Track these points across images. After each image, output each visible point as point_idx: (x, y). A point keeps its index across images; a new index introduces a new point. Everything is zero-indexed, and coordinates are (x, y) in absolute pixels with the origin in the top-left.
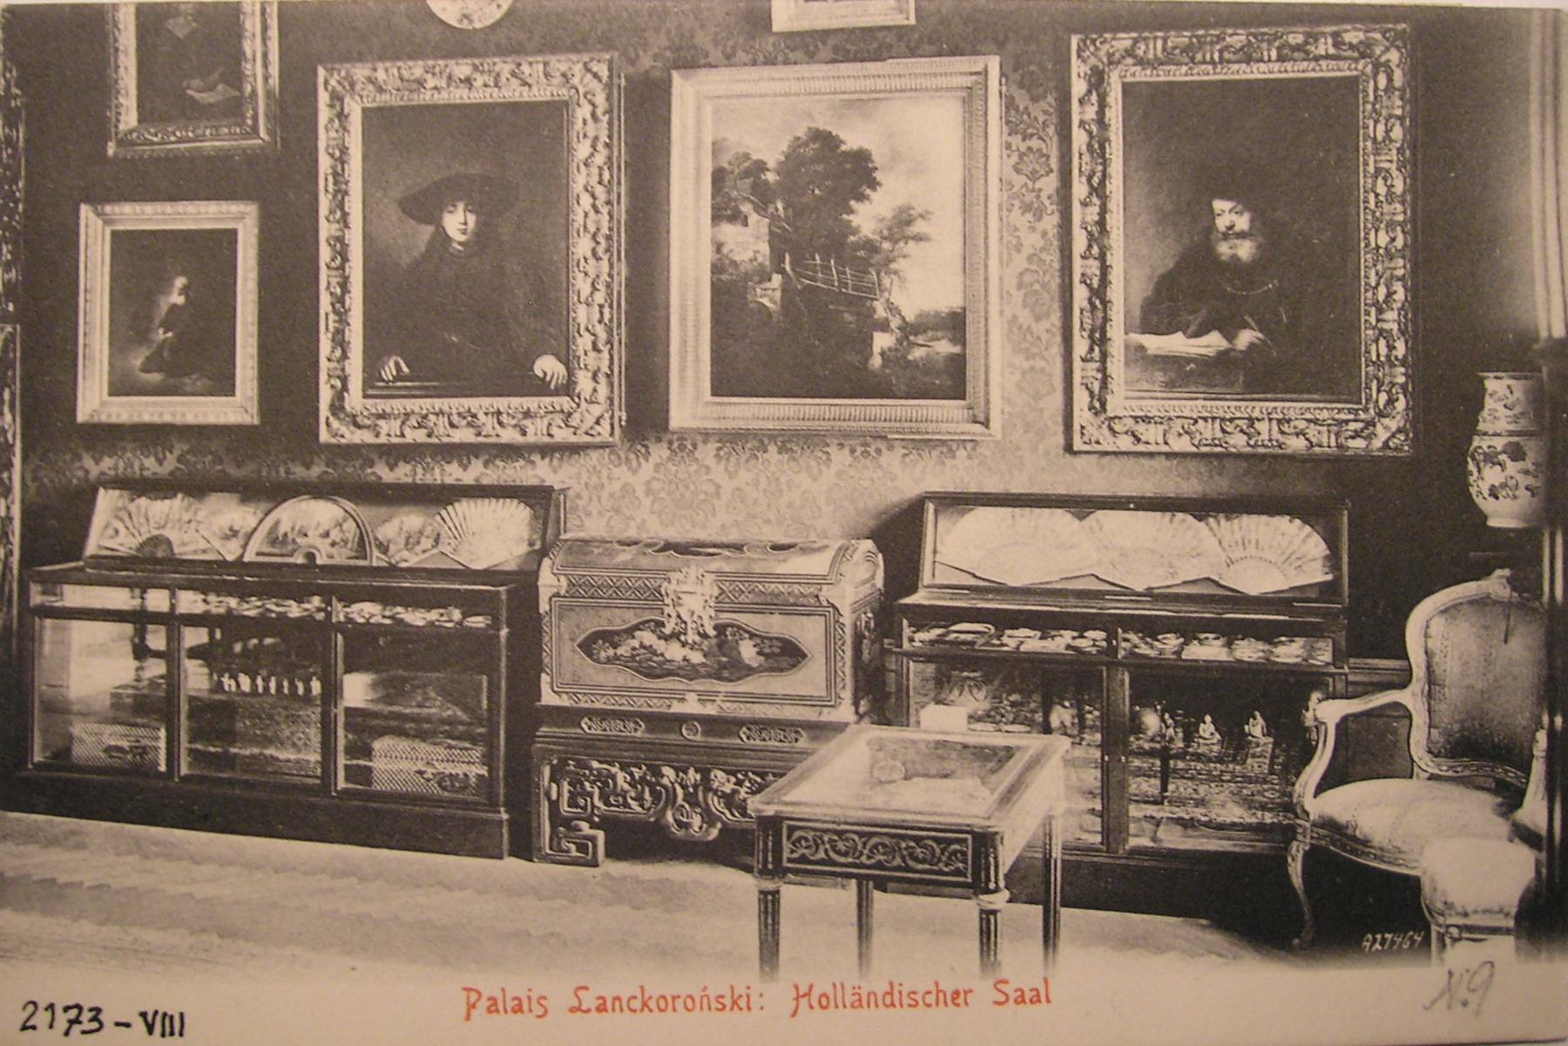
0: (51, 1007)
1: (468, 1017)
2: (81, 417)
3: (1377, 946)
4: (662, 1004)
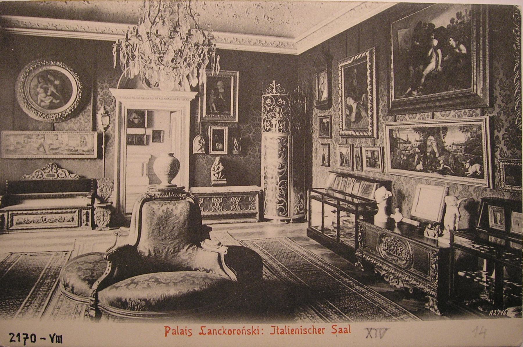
0: (19, 335)
1: (166, 335)
3: (495, 314)
4: (230, 332)
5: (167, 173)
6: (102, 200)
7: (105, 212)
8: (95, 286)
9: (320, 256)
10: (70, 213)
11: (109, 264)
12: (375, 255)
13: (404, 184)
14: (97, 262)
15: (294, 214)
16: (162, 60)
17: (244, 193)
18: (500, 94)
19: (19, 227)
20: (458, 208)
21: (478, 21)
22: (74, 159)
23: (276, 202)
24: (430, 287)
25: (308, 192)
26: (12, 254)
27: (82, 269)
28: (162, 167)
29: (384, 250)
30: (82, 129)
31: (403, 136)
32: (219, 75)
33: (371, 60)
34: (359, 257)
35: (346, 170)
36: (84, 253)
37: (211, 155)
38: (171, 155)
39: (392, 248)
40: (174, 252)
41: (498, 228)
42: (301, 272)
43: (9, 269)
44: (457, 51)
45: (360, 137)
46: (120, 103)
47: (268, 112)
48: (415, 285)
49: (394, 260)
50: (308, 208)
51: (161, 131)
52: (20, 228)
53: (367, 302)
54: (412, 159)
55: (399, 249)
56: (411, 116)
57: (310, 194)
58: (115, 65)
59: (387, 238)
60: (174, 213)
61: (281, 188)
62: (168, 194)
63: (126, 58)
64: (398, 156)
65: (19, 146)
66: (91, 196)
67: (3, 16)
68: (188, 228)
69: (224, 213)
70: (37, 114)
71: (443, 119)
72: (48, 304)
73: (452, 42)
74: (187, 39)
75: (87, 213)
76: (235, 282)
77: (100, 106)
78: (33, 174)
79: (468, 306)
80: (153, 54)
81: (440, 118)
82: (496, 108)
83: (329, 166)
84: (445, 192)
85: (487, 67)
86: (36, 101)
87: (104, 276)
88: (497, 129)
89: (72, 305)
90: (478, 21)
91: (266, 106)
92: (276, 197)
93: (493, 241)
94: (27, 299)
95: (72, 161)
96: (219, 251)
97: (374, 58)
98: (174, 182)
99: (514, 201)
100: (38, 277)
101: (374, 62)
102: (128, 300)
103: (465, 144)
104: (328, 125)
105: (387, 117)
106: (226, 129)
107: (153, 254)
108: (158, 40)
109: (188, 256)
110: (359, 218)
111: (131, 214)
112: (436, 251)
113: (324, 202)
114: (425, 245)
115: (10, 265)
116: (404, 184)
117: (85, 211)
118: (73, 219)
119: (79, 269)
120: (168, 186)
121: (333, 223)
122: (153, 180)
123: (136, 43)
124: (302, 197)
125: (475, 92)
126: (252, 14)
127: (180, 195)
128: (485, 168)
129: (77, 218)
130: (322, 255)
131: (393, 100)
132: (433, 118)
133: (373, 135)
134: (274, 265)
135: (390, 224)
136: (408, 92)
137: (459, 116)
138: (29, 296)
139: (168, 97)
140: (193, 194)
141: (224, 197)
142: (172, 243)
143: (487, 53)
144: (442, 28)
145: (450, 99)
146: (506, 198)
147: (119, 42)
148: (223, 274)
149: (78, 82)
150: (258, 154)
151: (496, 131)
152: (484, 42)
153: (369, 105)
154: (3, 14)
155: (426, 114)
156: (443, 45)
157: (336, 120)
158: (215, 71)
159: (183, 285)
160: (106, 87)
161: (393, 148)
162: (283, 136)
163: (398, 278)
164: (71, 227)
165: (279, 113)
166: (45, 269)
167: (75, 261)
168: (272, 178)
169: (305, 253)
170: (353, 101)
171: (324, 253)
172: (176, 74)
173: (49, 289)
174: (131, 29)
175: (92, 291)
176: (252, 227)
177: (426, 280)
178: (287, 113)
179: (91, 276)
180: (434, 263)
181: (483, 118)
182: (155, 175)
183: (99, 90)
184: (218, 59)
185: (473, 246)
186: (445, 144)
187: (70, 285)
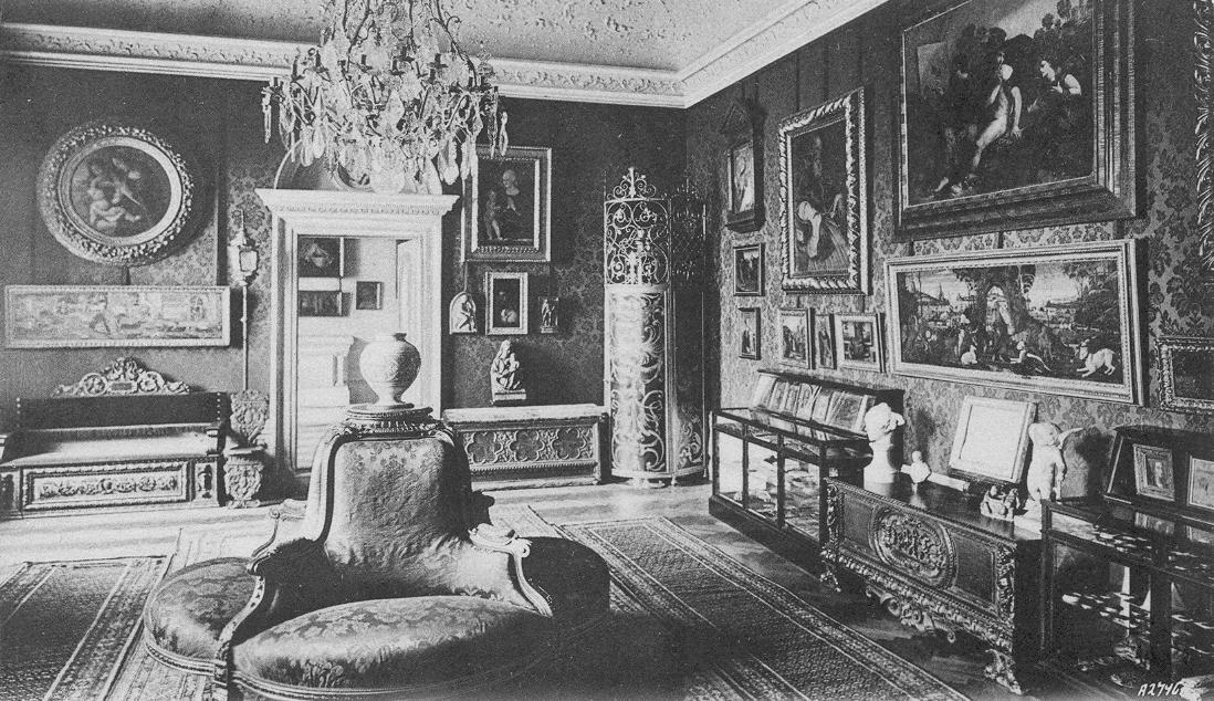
5: (392, 378)
6: (242, 440)
7: (249, 468)
8: (227, 633)
9: (741, 560)
10: (168, 469)
11: (259, 582)
12: (866, 558)
13: (932, 398)
14: (231, 579)
15: (679, 467)
16: (376, 124)
17: (565, 421)
18: (1162, 186)
19: (48, 503)
20: (1062, 451)
21: (1109, 19)
22: (175, 348)
23: (639, 441)
24: (996, 629)
25: (710, 417)
26: (30, 564)
27: (197, 596)
28: (378, 366)
29: (887, 545)
30: (195, 282)
31: (929, 288)
32: (506, 156)
33: (855, 119)
34: (829, 560)
35: (798, 366)
36: (200, 560)
37: (490, 336)
38: (400, 337)
39: (906, 540)
40: (408, 553)
41: (1156, 496)
42: (695, 594)
43: (25, 600)
44: (1060, 89)
45: (830, 292)
46: (282, 222)
47: (619, 238)
48: (960, 624)
49: (911, 568)
50: (710, 453)
51: (376, 283)
52: (50, 506)
53: (849, 662)
54: (953, 340)
55: (923, 542)
56: (947, 242)
57: (714, 420)
58: (268, 137)
59: (893, 518)
60: (408, 467)
61: (650, 407)
62: (393, 426)
63: (294, 119)
64: (917, 334)
65: (46, 321)
66: (216, 433)
67: (6, 25)
68: (441, 499)
69: (521, 464)
70: (90, 246)
71: (1024, 247)
72: (116, 677)
73: (1047, 70)
74: (433, 77)
75: (208, 470)
76: (549, 619)
77: (235, 228)
78: (81, 384)
79: (1087, 672)
80: (355, 110)
81: (1018, 246)
82: (1154, 218)
83: (759, 358)
84: (1028, 415)
85: (1131, 124)
86: (86, 218)
87: (248, 610)
88: (1156, 268)
89: (172, 678)
90: (1109, 19)
91: (613, 225)
92: (638, 429)
93: (1145, 524)
94: (67, 667)
95: (173, 353)
96: (510, 549)
97: (862, 111)
98: (407, 398)
99: (1196, 435)
100: (91, 617)
101: (863, 120)
102: (302, 664)
103: (1077, 304)
104: (755, 266)
105: (892, 246)
106: (524, 278)
107: (360, 558)
108: (366, 79)
109: (439, 565)
110: (828, 475)
111: (310, 470)
112: (1009, 548)
113: (747, 439)
114: (983, 535)
115: (26, 589)
116: (932, 398)
117: (203, 466)
118: (175, 483)
119: (190, 596)
120: (394, 407)
121: (769, 485)
122: (359, 393)
123: (315, 84)
124: (697, 428)
125: (1102, 184)
126: (581, 18)
127: (421, 427)
128: (1124, 359)
129: (185, 480)
130: (744, 556)
131: (906, 206)
132: (1001, 246)
133: (859, 286)
134: (635, 579)
135: (901, 487)
136: (940, 187)
137: (1062, 240)
138: (71, 660)
139: (394, 208)
140: (451, 424)
141: (520, 431)
142: (404, 534)
143: (1132, 93)
144: (1022, 38)
145: (1045, 201)
146: (1176, 426)
147: (276, 83)
148: (521, 600)
149: (183, 174)
150: (595, 332)
151: (1151, 273)
152: (1124, 65)
153: (851, 220)
154: (5, 19)
155: (985, 237)
156: (1026, 78)
157: (774, 253)
158: (497, 148)
159: (430, 626)
160: (249, 186)
161: (907, 316)
162: (653, 291)
163: (921, 608)
164: (171, 502)
165: (643, 240)
166: (110, 597)
167: (181, 577)
168: (629, 386)
169: (705, 553)
170: (813, 211)
171: (748, 551)
172: (409, 155)
173: (119, 644)
174: (304, 54)
175: (219, 644)
176: (586, 496)
177: (987, 613)
178: (663, 240)
179: (219, 611)
180: (1006, 576)
181: (1121, 243)
182: (363, 382)
183: (232, 191)
184: (504, 121)
185: (1098, 537)
186: (1030, 306)
187: (169, 632)
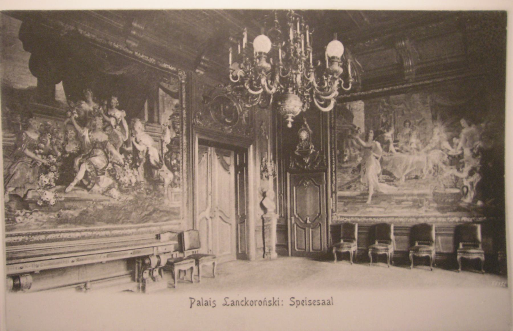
2: (30, 54)
4: (252, 304)
